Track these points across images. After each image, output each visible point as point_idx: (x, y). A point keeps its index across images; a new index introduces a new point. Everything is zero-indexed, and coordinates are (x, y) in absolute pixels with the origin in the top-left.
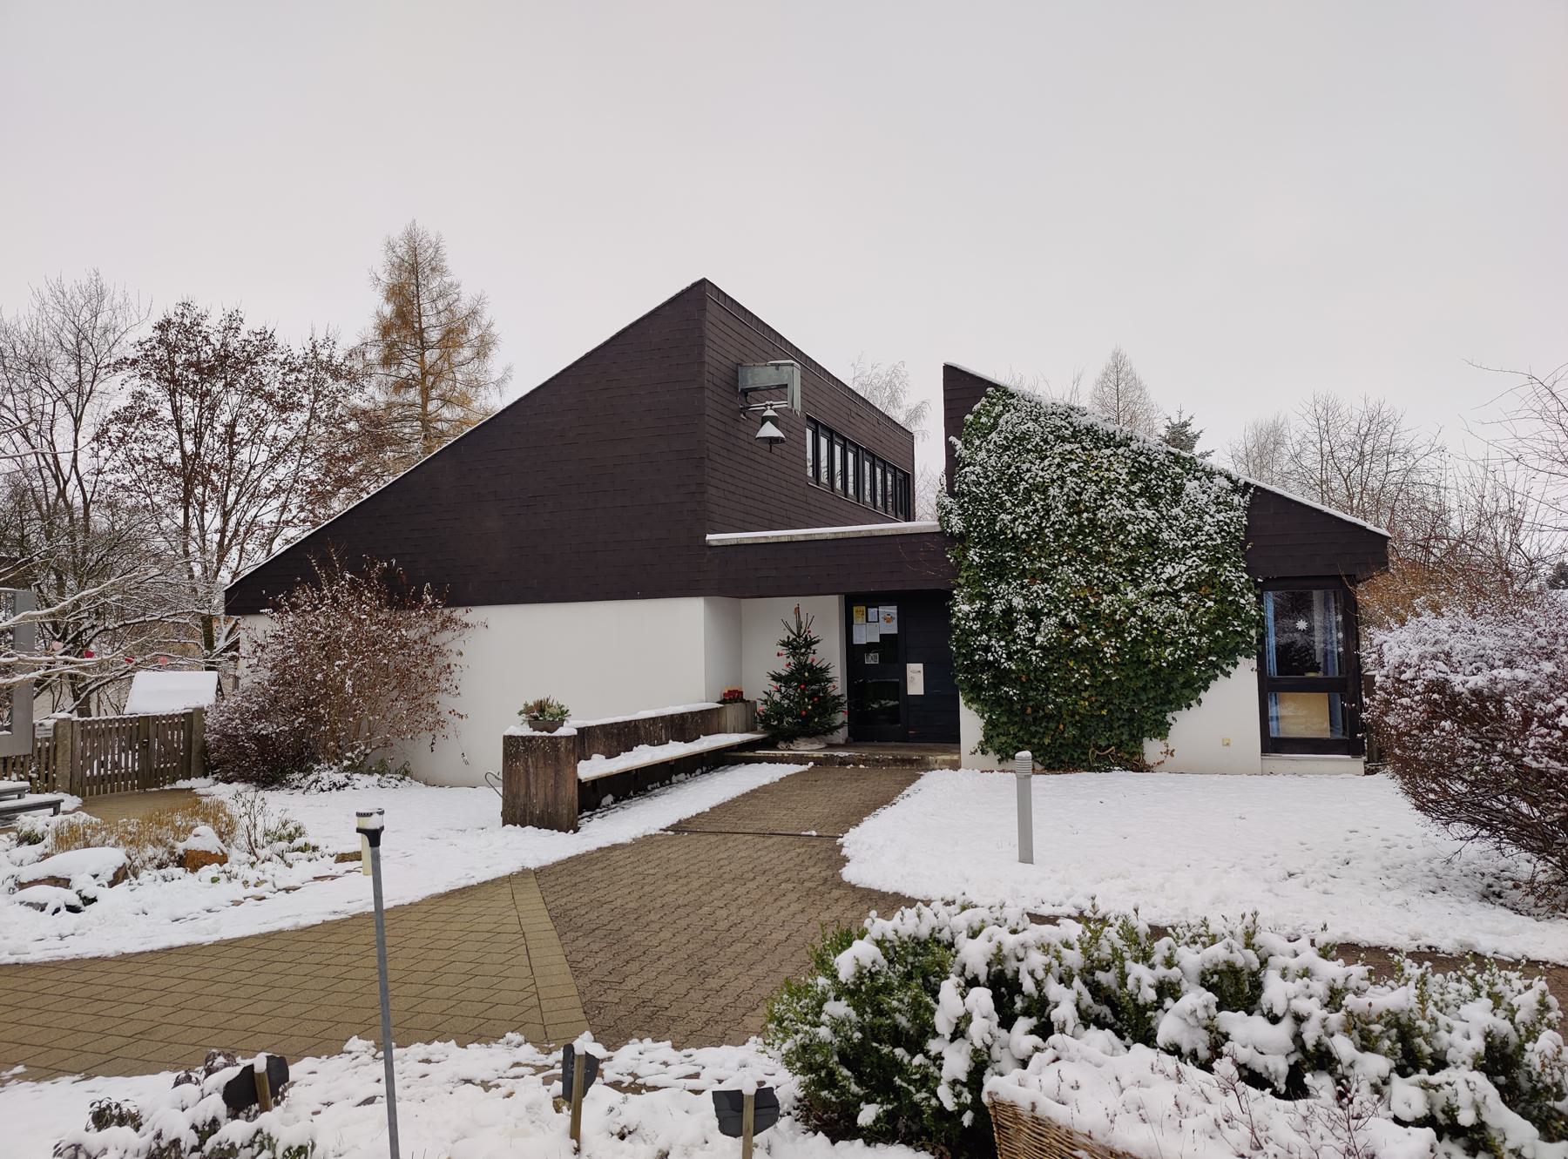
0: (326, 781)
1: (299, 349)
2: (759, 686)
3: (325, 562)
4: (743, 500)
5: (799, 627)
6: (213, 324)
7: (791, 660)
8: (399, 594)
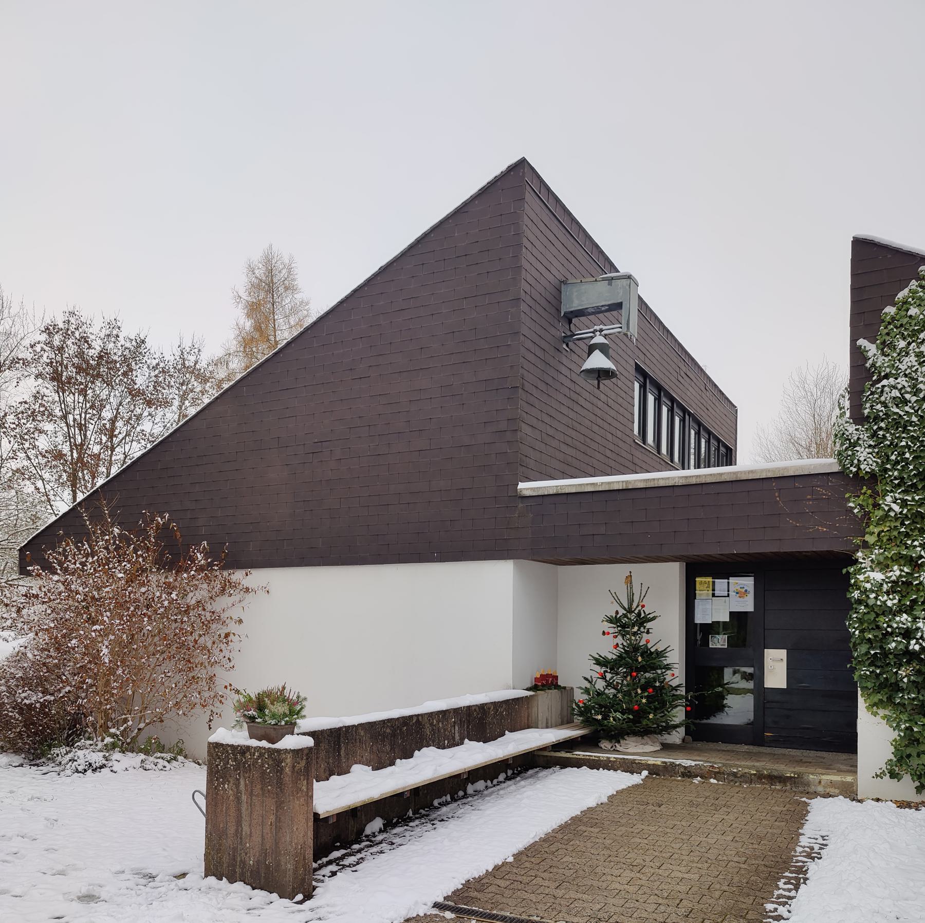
0: (81, 761)
1: (170, 355)
2: (579, 671)
3: (97, 518)
4: (564, 448)
5: (631, 602)
6: (96, 332)
7: (620, 640)
8: (172, 556)
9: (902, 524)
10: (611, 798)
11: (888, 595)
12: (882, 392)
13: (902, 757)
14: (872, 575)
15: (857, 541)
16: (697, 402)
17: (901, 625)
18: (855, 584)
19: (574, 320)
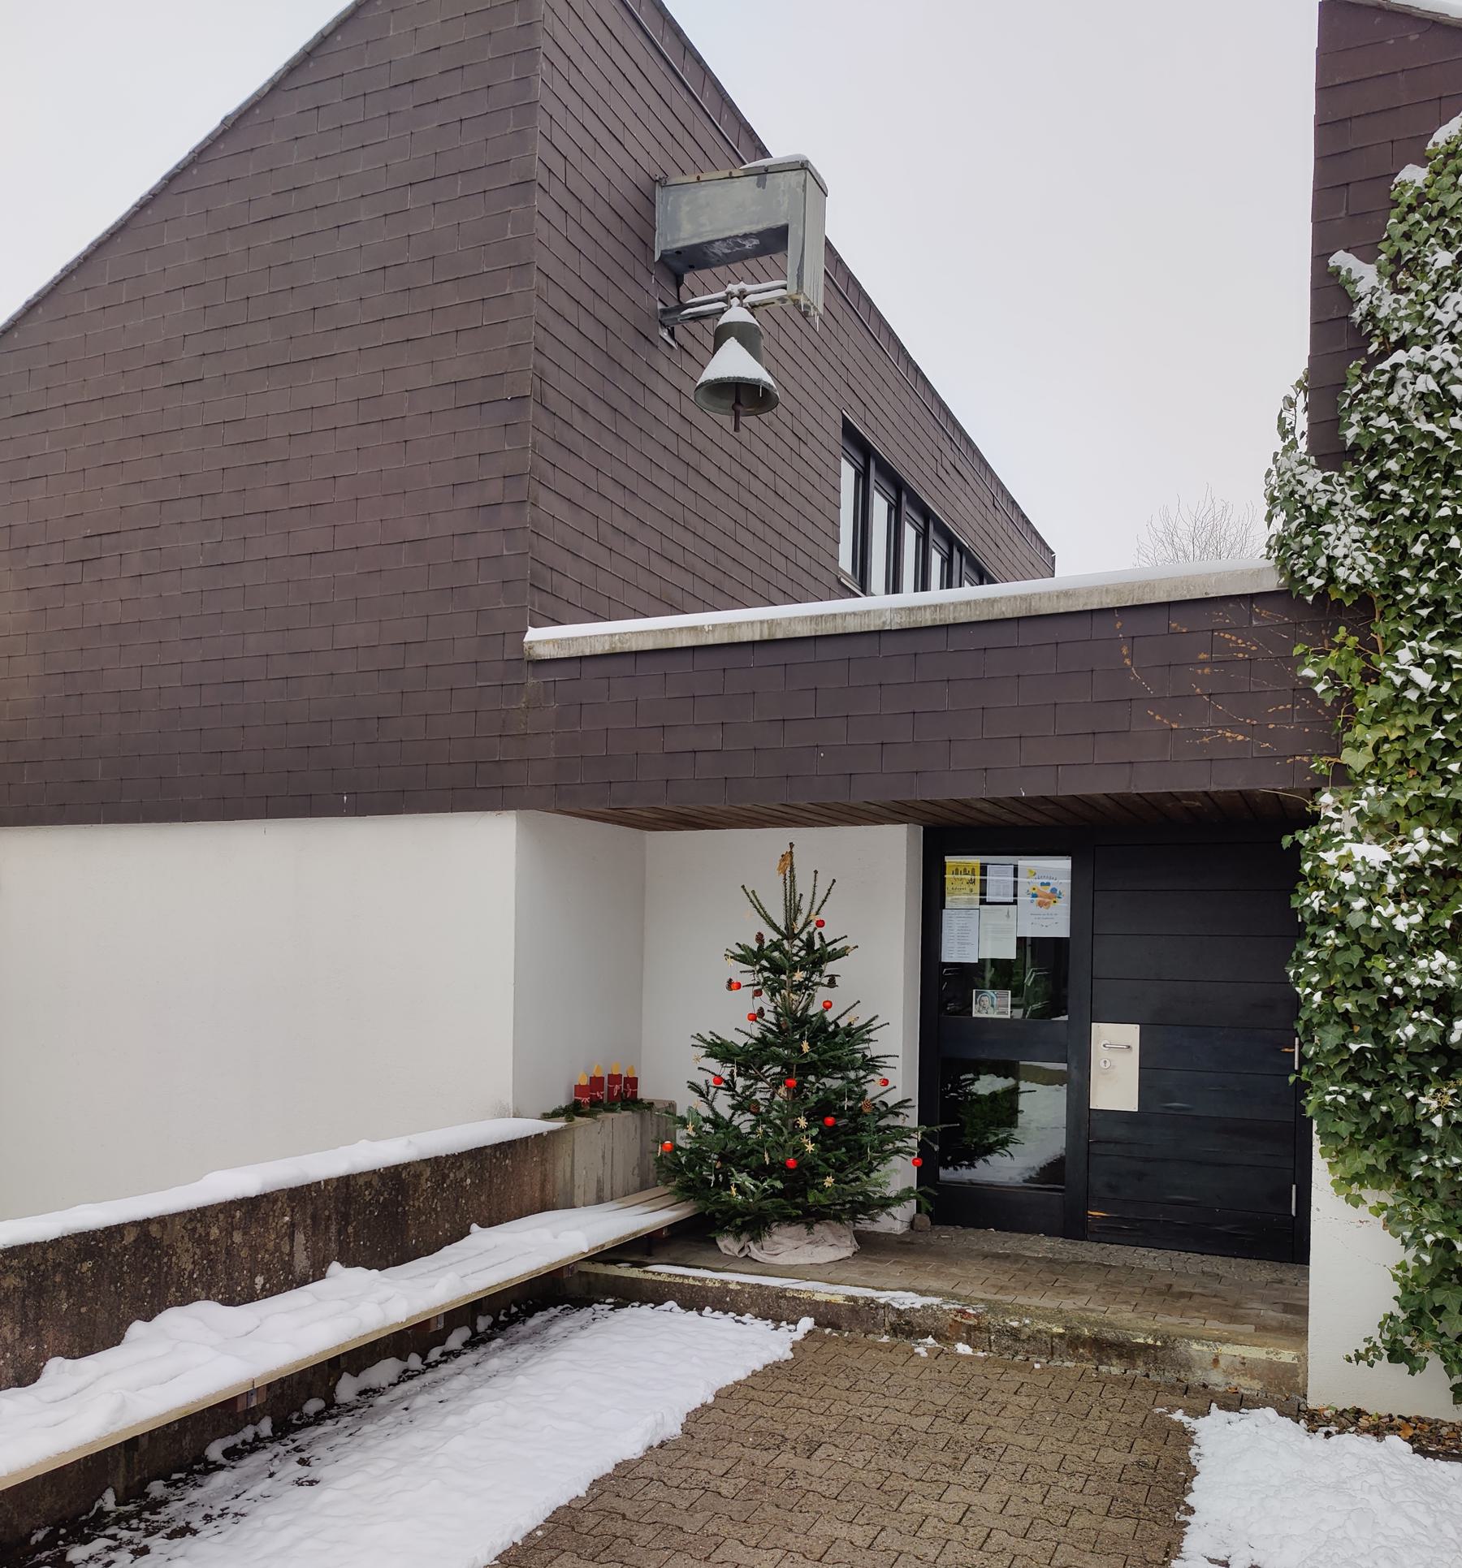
4: (658, 565)
5: (792, 910)
7: (764, 1001)
9: (1438, 721)
10: (697, 1417)
11: (1398, 903)
12: (1392, 381)
13: (1420, 1311)
14: (1359, 851)
15: (1321, 765)
16: (976, 527)
17: (1429, 981)
18: (1314, 875)
19: (688, 278)
